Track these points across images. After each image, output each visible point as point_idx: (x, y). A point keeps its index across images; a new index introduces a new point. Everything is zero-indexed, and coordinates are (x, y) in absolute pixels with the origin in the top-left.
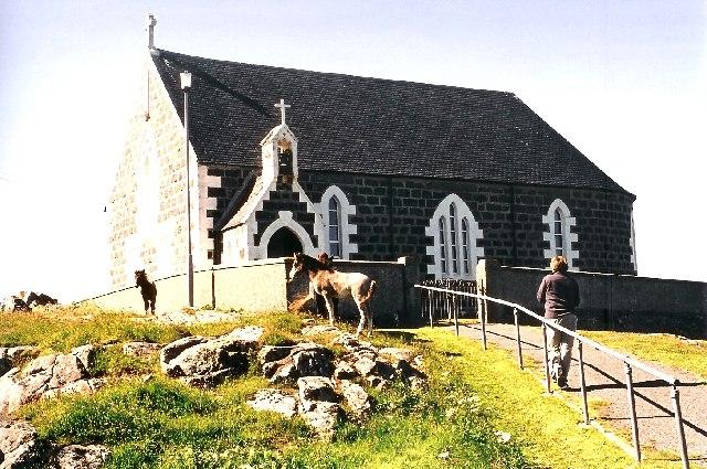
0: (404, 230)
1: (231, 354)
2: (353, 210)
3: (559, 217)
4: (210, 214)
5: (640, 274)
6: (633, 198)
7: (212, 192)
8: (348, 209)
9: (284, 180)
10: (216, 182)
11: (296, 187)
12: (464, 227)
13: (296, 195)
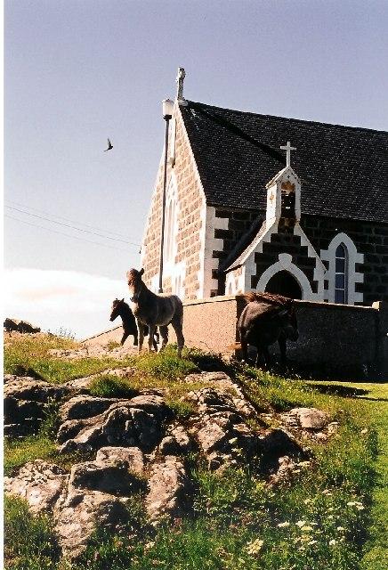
1: (22, 403)
2: (360, 258)
5: (363, 274)
7: (219, 234)
8: (355, 257)
9: (286, 224)
10: (224, 224)
11: (298, 230)
13: (298, 239)
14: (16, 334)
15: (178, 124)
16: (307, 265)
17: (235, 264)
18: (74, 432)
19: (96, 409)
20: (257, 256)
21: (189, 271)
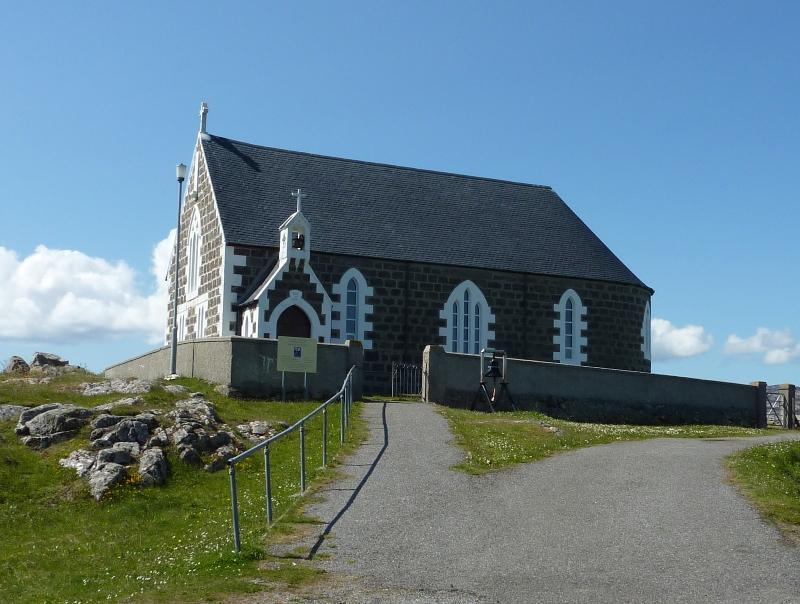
0: (418, 312)
2: (370, 291)
3: (571, 311)
4: (235, 289)
6: (652, 292)
7: (238, 270)
8: (365, 290)
10: (242, 261)
12: (477, 311)
14: (786, 393)
15: (198, 157)
16: (316, 301)
17: (250, 300)
18: (101, 435)
19: (113, 422)
20: (270, 292)
21: (211, 303)
